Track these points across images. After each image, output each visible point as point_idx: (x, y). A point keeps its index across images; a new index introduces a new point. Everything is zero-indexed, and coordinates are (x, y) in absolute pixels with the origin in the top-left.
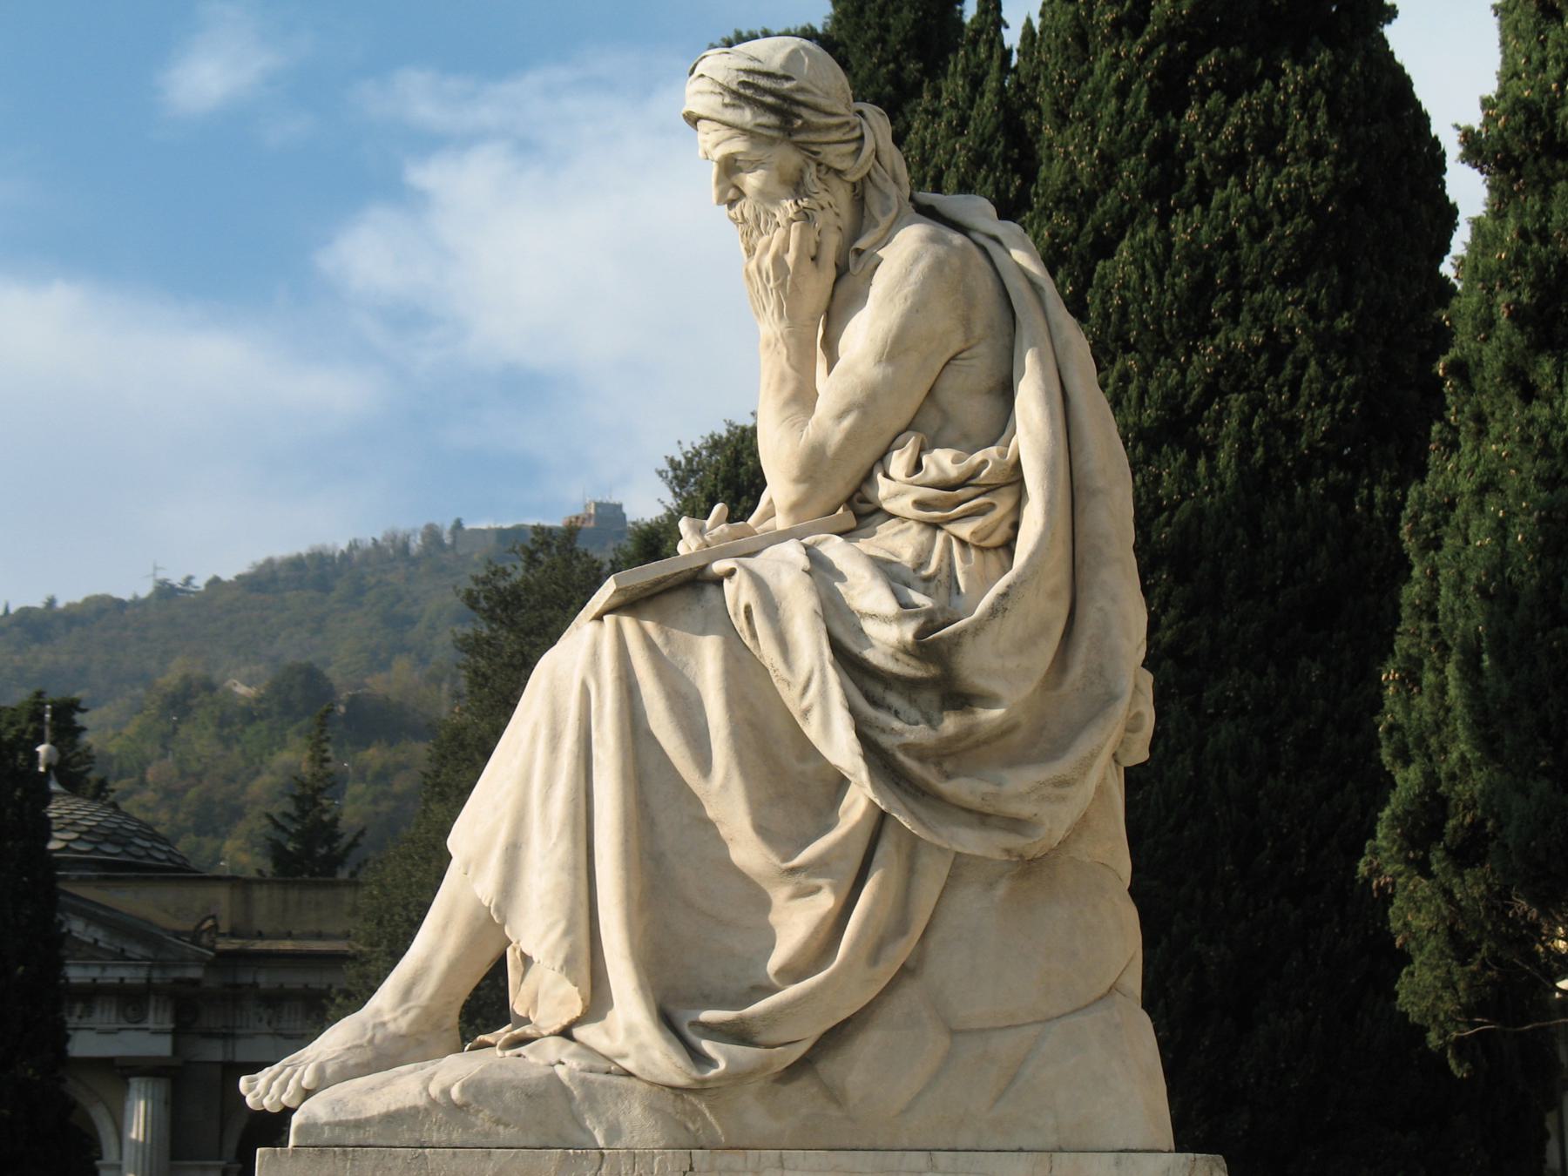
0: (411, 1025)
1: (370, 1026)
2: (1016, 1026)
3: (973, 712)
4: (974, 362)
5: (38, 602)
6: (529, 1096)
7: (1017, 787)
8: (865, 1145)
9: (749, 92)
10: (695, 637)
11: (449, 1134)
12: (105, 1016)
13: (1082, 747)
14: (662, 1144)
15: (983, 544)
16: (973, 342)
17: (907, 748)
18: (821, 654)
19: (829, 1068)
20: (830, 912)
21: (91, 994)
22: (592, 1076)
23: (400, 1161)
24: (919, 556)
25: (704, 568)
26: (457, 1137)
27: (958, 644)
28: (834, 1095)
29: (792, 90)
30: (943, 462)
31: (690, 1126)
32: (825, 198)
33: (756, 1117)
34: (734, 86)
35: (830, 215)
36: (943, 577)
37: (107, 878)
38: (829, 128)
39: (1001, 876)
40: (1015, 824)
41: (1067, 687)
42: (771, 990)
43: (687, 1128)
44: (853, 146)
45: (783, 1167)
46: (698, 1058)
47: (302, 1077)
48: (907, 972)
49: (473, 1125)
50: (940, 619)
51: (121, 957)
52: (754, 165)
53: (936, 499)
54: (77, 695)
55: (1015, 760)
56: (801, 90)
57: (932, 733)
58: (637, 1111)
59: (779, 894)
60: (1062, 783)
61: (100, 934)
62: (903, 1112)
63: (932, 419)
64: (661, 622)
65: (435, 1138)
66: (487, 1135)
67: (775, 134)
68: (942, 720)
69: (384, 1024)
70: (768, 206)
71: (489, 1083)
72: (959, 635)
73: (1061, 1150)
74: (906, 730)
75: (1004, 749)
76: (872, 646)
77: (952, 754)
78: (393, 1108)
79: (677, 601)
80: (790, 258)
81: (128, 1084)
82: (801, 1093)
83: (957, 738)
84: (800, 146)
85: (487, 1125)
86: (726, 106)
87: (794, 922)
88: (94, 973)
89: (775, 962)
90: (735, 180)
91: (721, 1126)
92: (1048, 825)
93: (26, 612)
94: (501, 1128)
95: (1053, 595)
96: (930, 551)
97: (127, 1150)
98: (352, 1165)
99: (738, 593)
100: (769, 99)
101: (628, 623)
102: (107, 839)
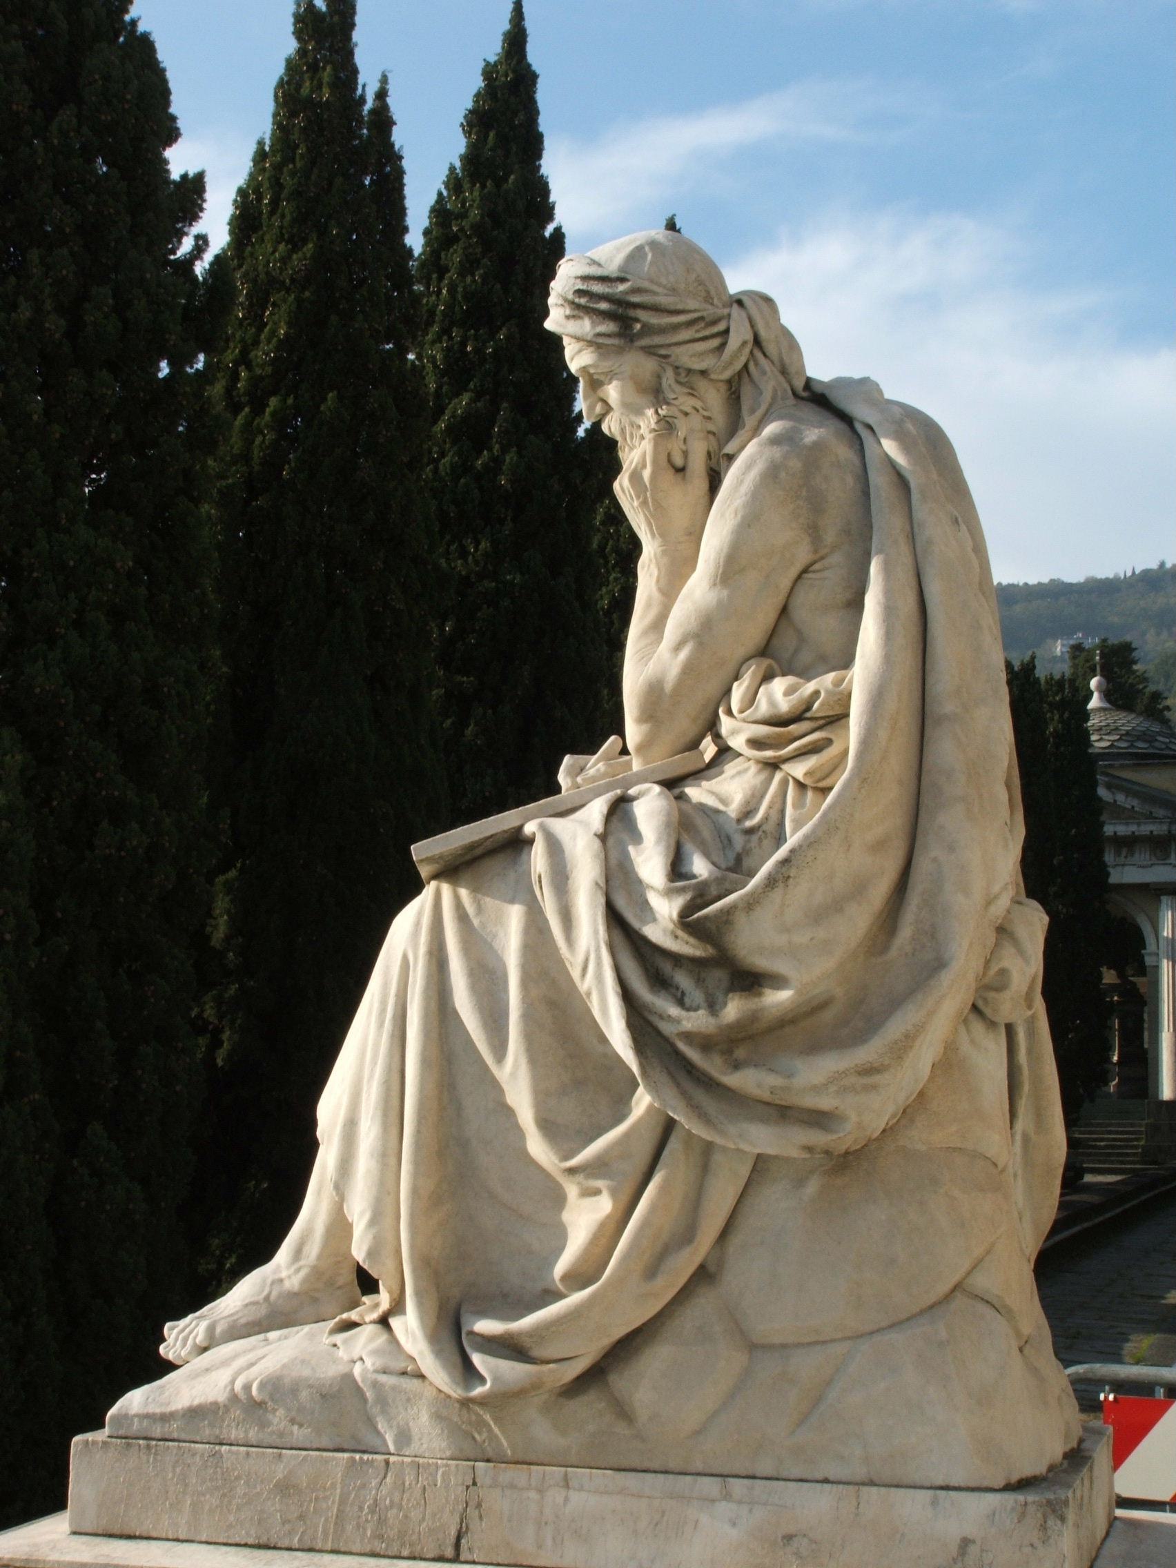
0: (305, 1280)
1: (269, 1281)
2: (824, 1342)
3: (760, 995)
4: (826, 574)
5: (1154, 565)
6: (323, 1396)
7: (813, 1077)
8: (655, 1465)
9: (583, 301)
10: (506, 905)
11: (246, 1432)
12: (1142, 856)
13: (895, 1029)
14: (448, 1454)
15: (821, 785)
16: (823, 552)
17: (688, 1036)
18: (596, 932)
19: (619, 1381)
20: (608, 1217)
21: (1127, 844)
22: (383, 1378)
23: (198, 1458)
24: (748, 803)
25: (521, 827)
26: (253, 1435)
27: (728, 922)
28: (623, 1412)
29: (626, 293)
30: (779, 694)
31: (477, 1436)
32: (687, 403)
33: (543, 1433)
34: (570, 296)
35: (696, 421)
36: (770, 827)
37: (1139, 765)
38: (676, 328)
39: (812, 1172)
40: (819, 1119)
41: (893, 952)
42: (559, 1296)
43: (474, 1438)
44: (715, 342)
45: (567, 1486)
46: (469, 1373)
47: (195, 1338)
48: (704, 1275)
49: (269, 1424)
50: (714, 891)
51: (1150, 817)
52: (611, 375)
53: (768, 737)
54: (1128, 638)
55: (814, 1047)
56: (637, 290)
57: (712, 1020)
58: (424, 1418)
59: (572, 1190)
60: (868, 1070)
61: (1135, 802)
62: (698, 1433)
63: (787, 642)
64: (475, 890)
65: (234, 1434)
66: (281, 1434)
67: (616, 341)
68: (725, 1004)
69: (281, 1280)
70: (633, 418)
71: (287, 1381)
72: (729, 912)
73: (872, 1483)
74: (684, 1019)
75: (808, 1029)
76: (655, 920)
77: (751, 1037)
78: (196, 1402)
79: (494, 865)
80: (646, 474)
81: (1160, 901)
82: (589, 1406)
83: (738, 1026)
84: (649, 351)
85: (282, 1426)
86: (568, 317)
87: (584, 1217)
88: (1133, 828)
89: (561, 1267)
90: (601, 394)
91: (507, 1438)
92: (854, 1118)
93: (1146, 572)
94: (296, 1427)
95: (878, 846)
96: (762, 796)
97: (1161, 942)
98: (155, 1459)
99: (538, 858)
100: (604, 306)
101: (446, 889)
102: (1139, 738)
